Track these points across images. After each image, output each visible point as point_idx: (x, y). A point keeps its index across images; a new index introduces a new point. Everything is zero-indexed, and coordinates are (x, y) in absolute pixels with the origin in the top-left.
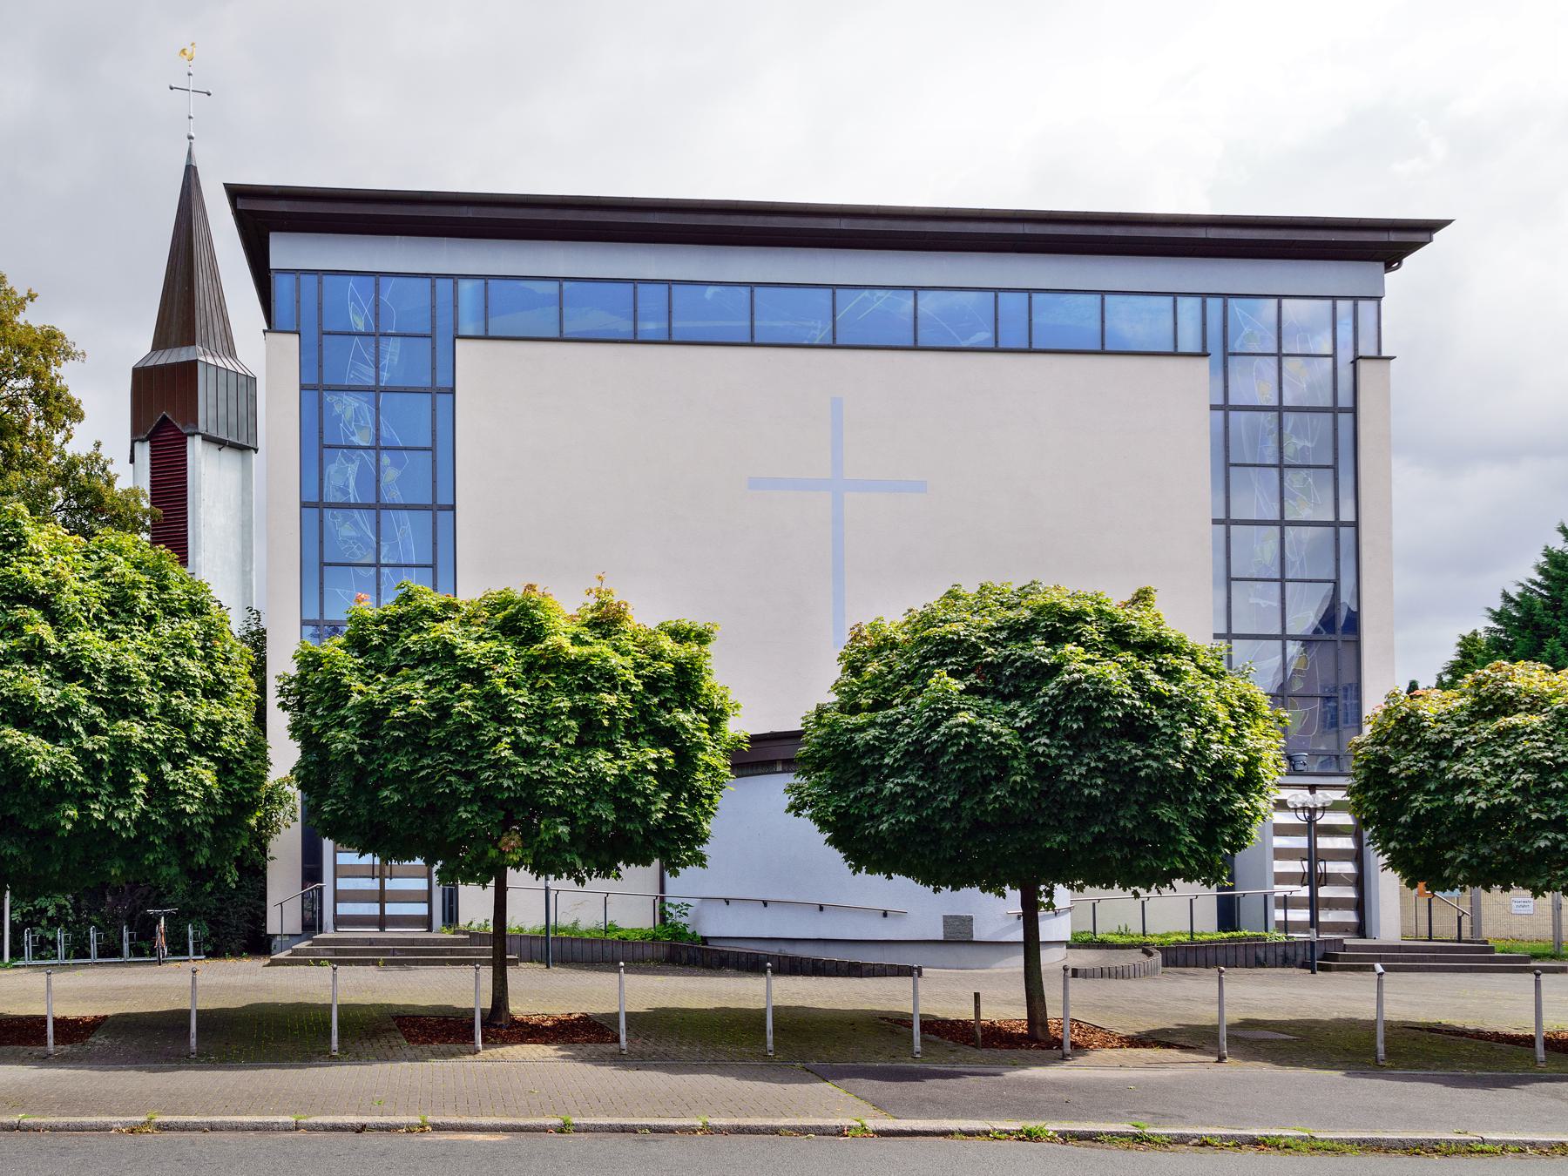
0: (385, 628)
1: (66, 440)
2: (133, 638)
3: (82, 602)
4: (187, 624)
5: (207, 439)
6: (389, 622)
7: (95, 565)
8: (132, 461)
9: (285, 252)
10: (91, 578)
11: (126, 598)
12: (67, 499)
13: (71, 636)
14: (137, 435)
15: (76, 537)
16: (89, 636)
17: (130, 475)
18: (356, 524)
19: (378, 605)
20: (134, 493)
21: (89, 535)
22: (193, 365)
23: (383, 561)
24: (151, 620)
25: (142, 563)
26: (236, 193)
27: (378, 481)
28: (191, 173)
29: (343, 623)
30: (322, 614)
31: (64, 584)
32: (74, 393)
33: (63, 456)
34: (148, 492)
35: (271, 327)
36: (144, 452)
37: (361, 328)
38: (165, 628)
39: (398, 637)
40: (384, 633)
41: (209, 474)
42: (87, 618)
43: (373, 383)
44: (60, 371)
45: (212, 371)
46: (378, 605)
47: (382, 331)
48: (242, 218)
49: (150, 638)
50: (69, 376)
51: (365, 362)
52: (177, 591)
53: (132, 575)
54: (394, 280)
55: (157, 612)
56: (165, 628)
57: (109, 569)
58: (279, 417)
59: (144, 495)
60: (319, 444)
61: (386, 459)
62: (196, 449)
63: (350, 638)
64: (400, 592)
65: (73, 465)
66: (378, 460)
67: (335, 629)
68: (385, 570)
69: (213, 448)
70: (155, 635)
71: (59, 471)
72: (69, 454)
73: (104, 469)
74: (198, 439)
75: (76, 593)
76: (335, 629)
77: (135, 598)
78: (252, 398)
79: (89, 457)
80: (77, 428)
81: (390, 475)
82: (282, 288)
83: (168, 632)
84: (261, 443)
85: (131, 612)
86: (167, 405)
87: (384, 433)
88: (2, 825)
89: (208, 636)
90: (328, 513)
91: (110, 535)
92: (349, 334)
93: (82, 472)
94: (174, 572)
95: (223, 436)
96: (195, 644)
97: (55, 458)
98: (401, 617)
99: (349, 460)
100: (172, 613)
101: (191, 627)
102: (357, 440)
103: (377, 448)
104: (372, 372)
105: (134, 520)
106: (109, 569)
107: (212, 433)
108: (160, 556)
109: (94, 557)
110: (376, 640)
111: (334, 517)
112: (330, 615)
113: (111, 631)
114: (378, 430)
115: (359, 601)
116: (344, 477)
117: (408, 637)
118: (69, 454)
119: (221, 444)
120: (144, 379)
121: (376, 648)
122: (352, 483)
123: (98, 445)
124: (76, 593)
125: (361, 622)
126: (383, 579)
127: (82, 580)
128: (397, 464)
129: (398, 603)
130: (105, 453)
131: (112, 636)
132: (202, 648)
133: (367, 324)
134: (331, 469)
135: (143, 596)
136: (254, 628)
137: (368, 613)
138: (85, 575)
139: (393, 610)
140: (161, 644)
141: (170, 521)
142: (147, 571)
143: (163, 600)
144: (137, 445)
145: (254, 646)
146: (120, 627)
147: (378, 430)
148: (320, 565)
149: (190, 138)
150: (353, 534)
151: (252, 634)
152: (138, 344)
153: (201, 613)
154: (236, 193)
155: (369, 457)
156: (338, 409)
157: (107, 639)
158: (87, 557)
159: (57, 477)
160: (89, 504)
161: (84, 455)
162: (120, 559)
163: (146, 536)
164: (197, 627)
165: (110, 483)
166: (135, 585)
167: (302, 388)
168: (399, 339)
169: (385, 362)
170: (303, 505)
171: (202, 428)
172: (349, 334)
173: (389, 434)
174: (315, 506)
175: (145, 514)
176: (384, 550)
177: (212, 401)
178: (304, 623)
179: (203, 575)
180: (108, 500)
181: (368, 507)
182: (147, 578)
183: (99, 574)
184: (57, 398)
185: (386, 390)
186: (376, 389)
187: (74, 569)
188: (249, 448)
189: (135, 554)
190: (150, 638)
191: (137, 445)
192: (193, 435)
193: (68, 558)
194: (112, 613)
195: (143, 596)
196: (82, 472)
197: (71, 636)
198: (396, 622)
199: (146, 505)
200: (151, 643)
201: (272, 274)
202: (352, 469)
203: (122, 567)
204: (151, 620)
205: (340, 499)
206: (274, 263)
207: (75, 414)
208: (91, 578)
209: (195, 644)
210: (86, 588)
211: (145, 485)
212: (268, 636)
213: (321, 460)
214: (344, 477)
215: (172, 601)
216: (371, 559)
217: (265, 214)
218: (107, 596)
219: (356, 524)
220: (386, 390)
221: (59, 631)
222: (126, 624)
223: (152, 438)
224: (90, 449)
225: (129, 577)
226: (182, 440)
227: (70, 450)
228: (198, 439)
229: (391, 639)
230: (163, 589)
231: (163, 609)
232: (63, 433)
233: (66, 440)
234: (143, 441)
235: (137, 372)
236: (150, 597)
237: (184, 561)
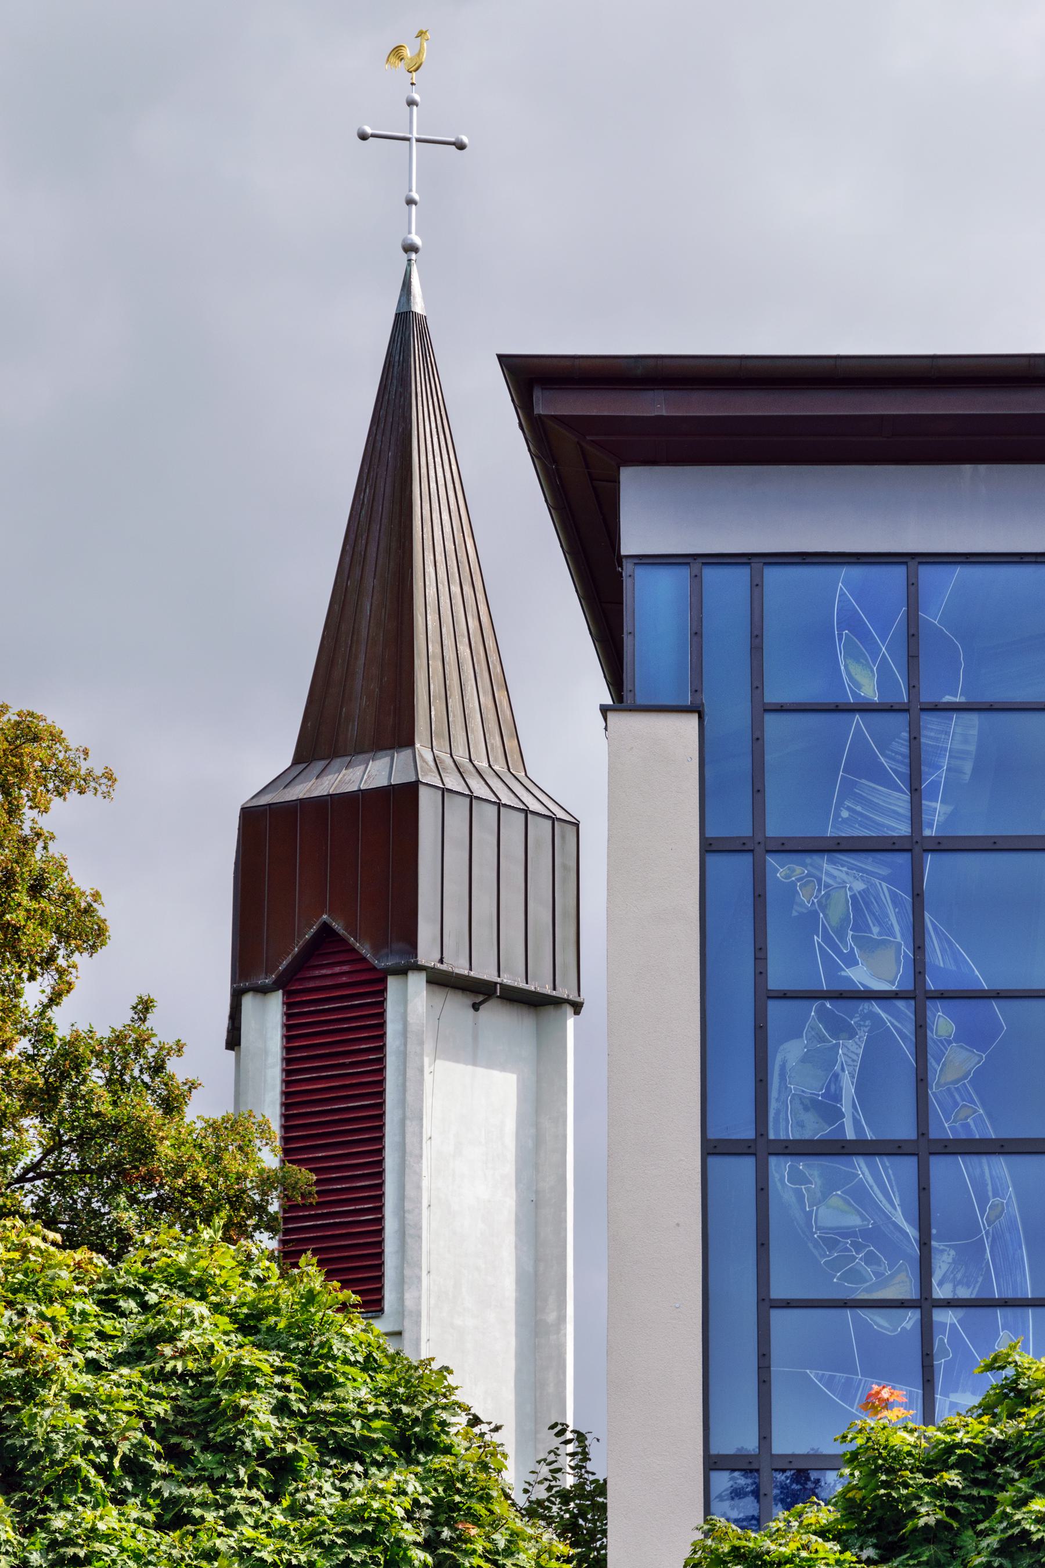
0: (952, 1478)
1: (55, 999)
2: (232, 1521)
3: (92, 1426)
4: (386, 1480)
5: (442, 981)
6: (964, 1464)
7: (132, 1326)
8: (233, 1041)
9: (654, 516)
10: (119, 1360)
11: (215, 1415)
12: (55, 1145)
13: (59, 1521)
14: (247, 975)
15: (81, 1254)
16: (109, 1519)
17: (227, 1080)
18: (860, 1197)
19: (928, 1418)
20: (233, 1130)
21: (115, 1244)
22: (410, 791)
23: (940, 1293)
24: (284, 1469)
25: (260, 1315)
26: (530, 378)
27: (922, 1081)
28: (406, 327)
29: (832, 1463)
30: (765, 1438)
31: (46, 1378)
32: (81, 878)
33: (43, 1036)
34: (276, 1125)
35: (623, 695)
36: (267, 1019)
37: (870, 691)
38: (323, 1493)
39: (992, 1503)
40: (952, 1493)
41: (457, 1118)
42: (104, 1471)
43: (903, 829)
44: (45, 823)
45: (457, 810)
46: (928, 1418)
47: (926, 697)
48: (543, 437)
49: (280, 1519)
50: (68, 832)
51: (880, 776)
52: (358, 1391)
53: (232, 1351)
54: (958, 572)
55: (305, 1448)
56: (323, 1493)
57: (169, 1336)
58: (638, 924)
59: (263, 1129)
60: (748, 1000)
61: (942, 1023)
62: (410, 1003)
63: (850, 1507)
64: (994, 1379)
65: (70, 1060)
66: (921, 1027)
67: (799, 1483)
68: (945, 1318)
69: (457, 1006)
70: (295, 1511)
71: (33, 1076)
72: (62, 1032)
73: (157, 1069)
74: (417, 982)
75: (77, 1401)
76: (799, 1483)
77: (241, 1412)
78: (567, 874)
79: (119, 1039)
80: (84, 967)
81: (954, 1064)
82: (653, 604)
83: (330, 1503)
84: (594, 988)
85: (228, 1449)
86: (330, 901)
87: (937, 955)
88: (1042, 1475)
89: (444, 1511)
90: (780, 1169)
91: (169, 1246)
92: (837, 709)
93: (96, 1077)
94: (350, 1334)
95: (485, 972)
96: (409, 1533)
97: (24, 1044)
98: (998, 1451)
99: (841, 1029)
100: (348, 1451)
101: (398, 1489)
102: (861, 975)
103: (918, 995)
104: (901, 802)
105: (236, 1201)
106: (169, 1336)
107: (458, 965)
108: (311, 1297)
109: (129, 1304)
110: (928, 1514)
111: (798, 1178)
112: (790, 1440)
113: (174, 1501)
114: (919, 947)
115: (874, 1405)
116: (817, 1072)
117: (1022, 1502)
118: (62, 1032)
119: (479, 992)
120: (273, 843)
121: (929, 1535)
122: (848, 1088)
123: (144, 1007)
124: (77, 1401)
125: (879, 1463)
126: (941, 1340)
127: (94, 1367)
128: (971, 1036)
129: (987, 1408)
130: (162, 1027)
131: (173, 1518)
132: (428, 1545)
133: (884, 680)
134: (789, 1054)
135: (260, 1407)
136: (569, 1481)
137: (902, 1440)
138: (100, 1352)
139: (973, 1432)
140: (311, 1538)
141: (338, 1203)
142: (269, 1341)
143: (318, 1417)
144: (248, 1002)
145: (569, 1530)
146: (196, 1492)
147: (919, 947)
148: (754, 1303)
149: (410, 248)
150: (853, 1220)
151: (565, 1497)
152: (260, 757)
153: (430, 1446)
154: (530, 378)
155: (897, 1021)
156: (806, 898)
157: (161, 1526)
158: (108, 1305)
159: (29, 1092)
160: (105, 1163)
161: (103, 1032)
162: (199, 1309)
163: (266, 1242)
164: (413, 1486)
165: (170, 1105)
166: (241, 1378)
167: (708, 847)
168: (974, 718)
169: (936, 776)
170: (712, 1149)
171: (427, 953)
172: (837, 709)
173: (951, 961)
174: (737, 1147)
175: (266, 1182)
176: (942, 1264)
177: (455, 887)
178: (712, 1463)
179: (431, 1342)
180: (165, 1149)
181: (892, 1149)
182: (275, 1358)
183: (140, 1351)
184: (36, 889)
185: (942, 846)
186: (914, 847)
187: (71, 1339)
188: (557, 1002)
189: (242, 1292)
190: (280, 1519)
191: (248, 1002)
192: (402, 972)
193: (57, 1310)
194: (174, 1454)
195: (260, 1407)
196: (96, 1077)
197: (59, 1521)
198: (986, 1464)
199: (270, 1159)
200: (283, 1533)
201: (628, 568)
202: (850, 1052)
203: (205, 1329)
204: (284, 1469)
205: (814, 1129)
206: (632, 542)
207: (83, 928)
208: (119, 1360)
209: (409, 1533)
210: (105, 1388)
211: (270, 1109)
212: (613, 1500)
213: (760, 1030)
214: (817, 1072)
215: (343, 1417)
216: (904, 1287)
217: (598, 426)
218: (161, 1408)
219: (860, 1197)
220: (942, 846)
221: (25, 1505)
222: (214, 1484)
223: (286, 983)
224: (122, 1017)
225: (226, 1355)
226: (375, 987)
227: (65, 1021)
228: (417, 982)
229: (972, 1509)
230: (318, 1385)
231: (320, 1441)
232: (46, 982)
233: (55, 999)
234: (264, 991)
235: (253, 819)
236: (281, 1409)
237: (373, 1305)
